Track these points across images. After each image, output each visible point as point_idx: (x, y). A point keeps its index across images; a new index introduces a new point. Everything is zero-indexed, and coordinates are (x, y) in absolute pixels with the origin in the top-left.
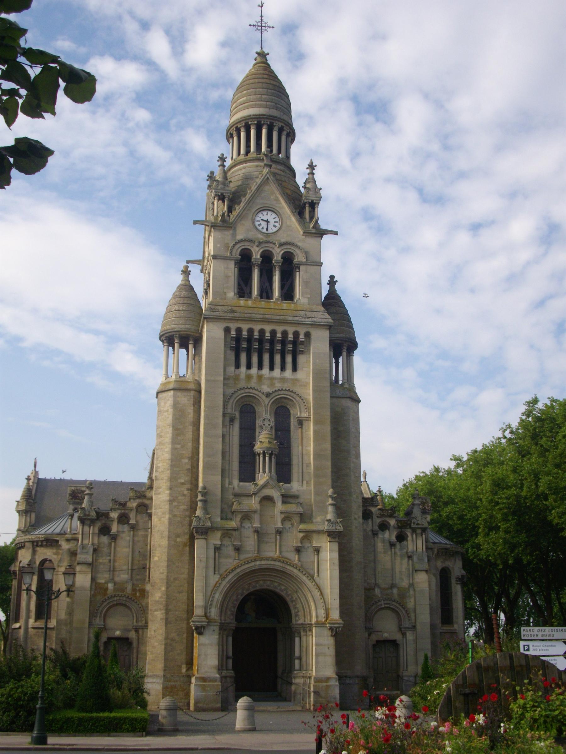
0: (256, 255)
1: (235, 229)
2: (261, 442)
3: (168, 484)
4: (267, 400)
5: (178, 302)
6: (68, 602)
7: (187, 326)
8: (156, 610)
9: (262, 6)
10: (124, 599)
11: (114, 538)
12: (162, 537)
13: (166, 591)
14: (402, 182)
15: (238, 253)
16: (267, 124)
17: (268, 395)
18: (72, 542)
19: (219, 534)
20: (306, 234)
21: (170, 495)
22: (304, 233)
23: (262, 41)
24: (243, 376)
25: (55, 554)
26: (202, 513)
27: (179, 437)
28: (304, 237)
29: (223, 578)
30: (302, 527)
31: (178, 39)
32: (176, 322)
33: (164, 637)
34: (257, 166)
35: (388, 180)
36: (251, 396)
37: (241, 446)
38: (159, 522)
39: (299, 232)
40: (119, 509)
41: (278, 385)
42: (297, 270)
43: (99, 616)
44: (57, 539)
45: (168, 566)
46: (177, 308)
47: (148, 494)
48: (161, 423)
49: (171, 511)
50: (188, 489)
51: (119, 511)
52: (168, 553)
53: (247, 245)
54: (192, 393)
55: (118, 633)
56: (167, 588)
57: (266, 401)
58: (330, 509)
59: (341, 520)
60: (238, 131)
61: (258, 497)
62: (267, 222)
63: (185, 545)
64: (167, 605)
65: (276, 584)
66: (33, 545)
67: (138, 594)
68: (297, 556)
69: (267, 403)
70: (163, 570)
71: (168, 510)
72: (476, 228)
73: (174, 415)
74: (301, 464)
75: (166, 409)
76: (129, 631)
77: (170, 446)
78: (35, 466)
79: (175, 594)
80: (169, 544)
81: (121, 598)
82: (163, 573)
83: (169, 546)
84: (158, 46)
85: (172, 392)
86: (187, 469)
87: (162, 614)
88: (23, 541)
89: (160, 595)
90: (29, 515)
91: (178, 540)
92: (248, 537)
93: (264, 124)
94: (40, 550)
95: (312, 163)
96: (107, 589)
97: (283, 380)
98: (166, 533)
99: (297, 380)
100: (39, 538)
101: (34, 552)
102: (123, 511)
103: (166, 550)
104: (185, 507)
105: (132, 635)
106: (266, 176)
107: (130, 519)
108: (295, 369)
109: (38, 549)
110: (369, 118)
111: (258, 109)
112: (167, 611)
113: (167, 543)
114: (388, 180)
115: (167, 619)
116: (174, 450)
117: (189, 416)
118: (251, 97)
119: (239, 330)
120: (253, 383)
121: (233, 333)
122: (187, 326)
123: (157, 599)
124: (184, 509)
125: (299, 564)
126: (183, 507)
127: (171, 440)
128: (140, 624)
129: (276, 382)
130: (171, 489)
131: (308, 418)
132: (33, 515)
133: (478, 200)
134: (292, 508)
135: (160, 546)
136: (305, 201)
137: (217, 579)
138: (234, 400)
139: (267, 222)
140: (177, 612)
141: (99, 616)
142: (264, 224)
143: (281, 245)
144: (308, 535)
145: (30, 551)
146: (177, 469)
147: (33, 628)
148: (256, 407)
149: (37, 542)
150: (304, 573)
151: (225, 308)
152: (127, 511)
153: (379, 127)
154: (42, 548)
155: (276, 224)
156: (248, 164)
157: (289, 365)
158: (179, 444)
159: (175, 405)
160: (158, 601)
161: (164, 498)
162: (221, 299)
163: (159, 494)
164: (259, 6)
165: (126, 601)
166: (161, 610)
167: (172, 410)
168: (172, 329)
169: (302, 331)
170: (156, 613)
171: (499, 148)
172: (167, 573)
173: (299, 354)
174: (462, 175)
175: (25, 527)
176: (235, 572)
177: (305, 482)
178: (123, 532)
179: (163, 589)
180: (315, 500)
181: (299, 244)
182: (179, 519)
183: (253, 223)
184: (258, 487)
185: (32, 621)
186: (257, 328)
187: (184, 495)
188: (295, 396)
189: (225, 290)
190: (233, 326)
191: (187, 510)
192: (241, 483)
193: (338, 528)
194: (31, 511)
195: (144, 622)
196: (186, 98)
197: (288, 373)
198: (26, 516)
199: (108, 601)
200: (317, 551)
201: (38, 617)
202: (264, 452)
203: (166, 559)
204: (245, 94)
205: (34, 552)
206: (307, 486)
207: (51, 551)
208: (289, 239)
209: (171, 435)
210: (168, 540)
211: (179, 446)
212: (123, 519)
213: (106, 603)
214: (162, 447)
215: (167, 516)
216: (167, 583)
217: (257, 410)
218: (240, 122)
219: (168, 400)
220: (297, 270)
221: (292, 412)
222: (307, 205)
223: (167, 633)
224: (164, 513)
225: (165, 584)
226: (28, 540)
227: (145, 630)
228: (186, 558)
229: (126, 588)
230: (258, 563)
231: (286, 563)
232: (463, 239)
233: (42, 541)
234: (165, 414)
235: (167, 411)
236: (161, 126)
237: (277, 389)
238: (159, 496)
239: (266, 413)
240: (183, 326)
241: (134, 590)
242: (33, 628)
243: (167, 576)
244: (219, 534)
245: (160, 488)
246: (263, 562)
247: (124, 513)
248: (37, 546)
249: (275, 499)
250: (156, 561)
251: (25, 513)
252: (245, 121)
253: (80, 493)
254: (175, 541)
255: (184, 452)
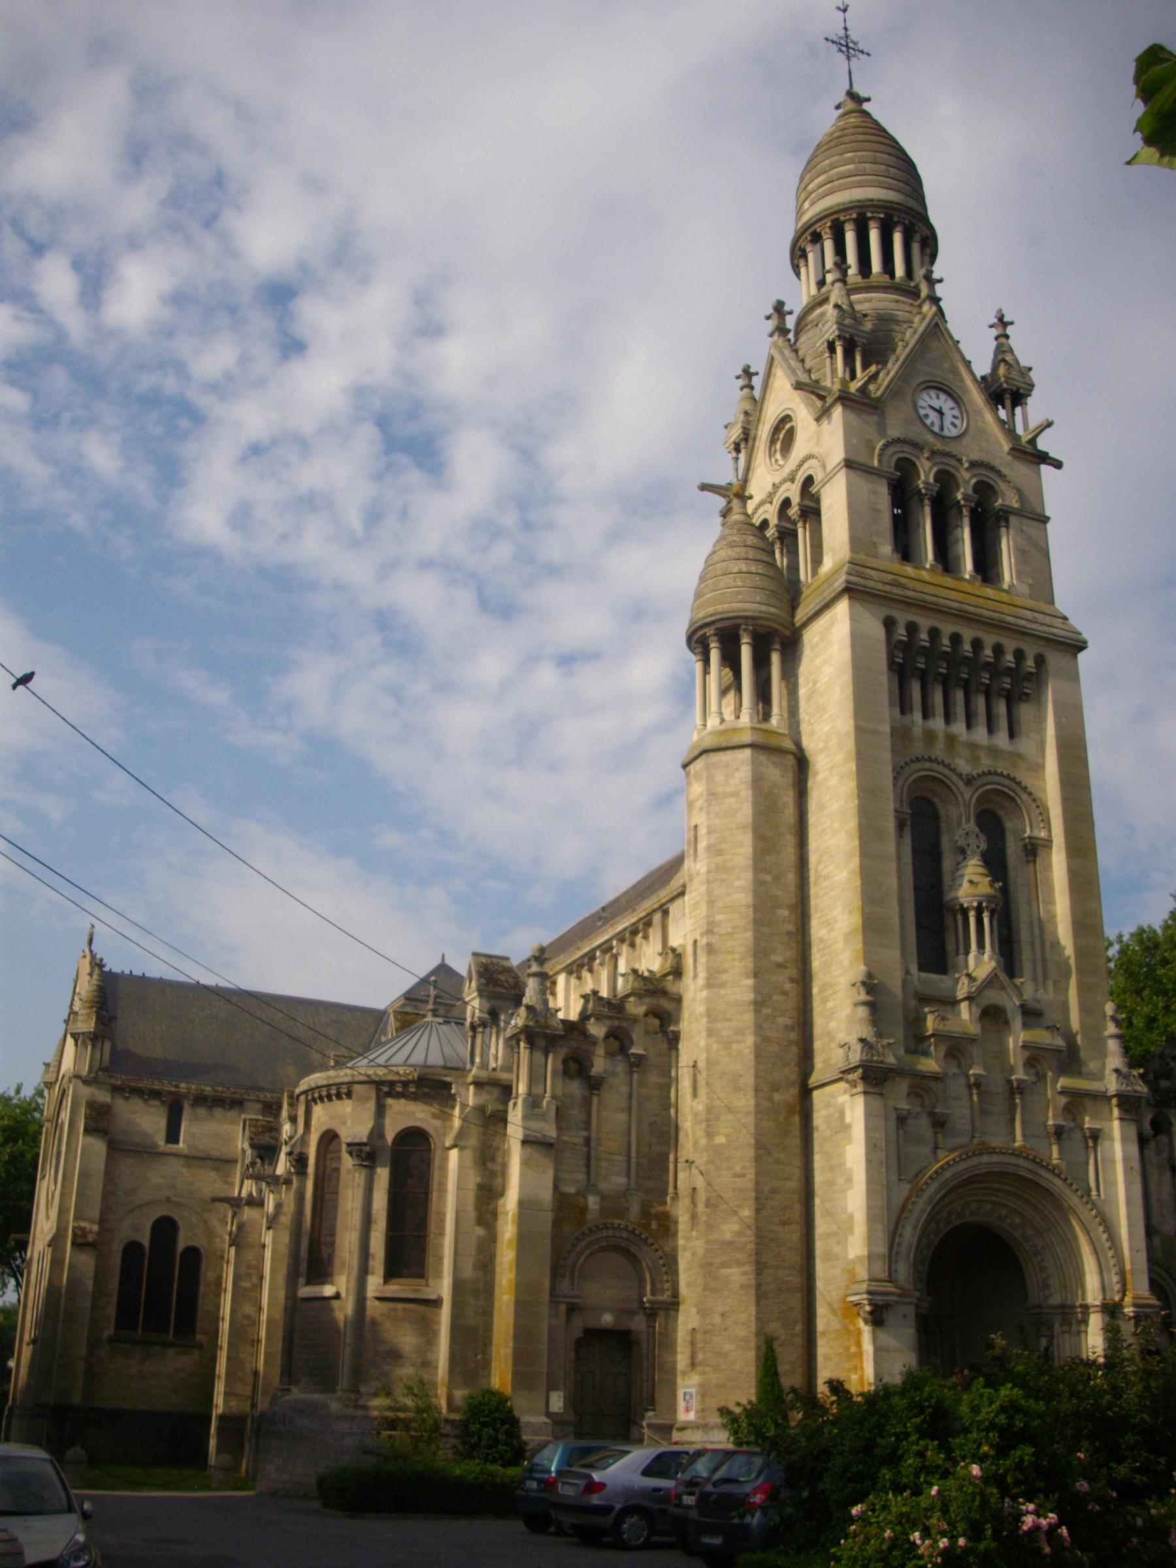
0: (926, 474)
1: (882, 415)
2: (971, 882)
3: (749, 963)
4: (967, 792)
5: (744, 556)
6: (479, 1237)
7: (772, 610)
8: (724, 1265)
9: (845, 11)
10: (625, 1234)
11: (594, 1085)
12: (738, 1089)
13: (757, 1219)
14: (448, 569)
15: (892, 464)
16: (904, 224)
17: (969, 781)
18: (488, 1088)
19: (903, 1086)
20: (1018, 455)
21: (756, 989)
22: (1013, 449)
23: (850, 73)
24: (917, 731)
25: (434, 1116)
26: (872, 1033)
27: (768, 858)
28: (1009, 458)
29: (918, 1191)
30: (1063, 1082)
31: (94, 280)
32: (747, 599)
33: (753, 1330)
34: (897, 301)
35: (426, 564)
36: (935, 778)
37: (917, 889)
38: (723, 1053)
39: (1001, 446)
40: (610, 1018)
41: (986, 763)
42: (1003, 523)
43: (568, 1275)
44: (448, 1079)
45: (757, 1159)
46: (744, 568)
47: (672, 988)
48: (717, 822)
49: (759, 1028)
50: (792, 980)
51: (608, 1022)
52: (757, 1127)
53: (908, 452)
54: (790, 761)
55: (607, 1319)
56: (758, 1211)
57: (968, 795)
58: (1113, 1046)
59: (1141, 1071)
60: (817, 238)
61: (977, 1006)
62: (940, 412)
63: (791, 1112)
64: (758, 1252)
65: (1004, 1212)
66: (378, 1091)
67: (654, 1225)
68: (1055, 1149)
69: (967, 797)
70: (743, 1167)
71: (752, 1024)
72: (568, 661)
73: (756, 804)
74: (1038, 941)
75: (731, 789)
76: (631, 1313)
77: (749, 876)
78: (90, 941)
79: (775, 1228)
80: (757, 1105)
81: (618, 1234)
82: (743, 1176)
83: (758, 1111)
84: (57, 283)
85: (748, 752)
86: (789, 933)
87: (745, 1273)
88: (346, 1079)
89: (735, 1227)
90: (99, 1045)
91: (777, 1097)
92: (956, 1098)
93: (897, 223)
94: (318, 1110)
95: (1003, 316)
96: (584, 1210)
97: (994, 751)
98: (749, 1079)
99: (1020, 756)
100: (398, 1073)
101: (380, 1111)
102: (616, 1023)
103: (751, 1120)
104: (789, 1022)
105: (638, 1323)
106: (932, 319)
107: (632, 1043)
108: (1012, 734)
109: (390, 1101)
110: (403, 459)
111: (884, 191)
112: (760, 1267)
113: (752, 1102)
114: (426, 564)
115: (758, 1286)
116: (759, 888)
117: (787, 811)
118: (867, 165)
119: (912, 628)
120: (939, 751)
121: (901, 633)
122: (772, 610)
123: (728, 1236)
124: (786, 1027)
125: (1064, 1166)
126: (782, 1021)
127: (750, 862)
128: (660, 1298)
129: (982, 754)
130: (756, 975)
131: (1048, 843)
132: (107, 1046)
133: (577, 617)
134: (1043, 1037)
135: (730, 1110)
136: (1005, 386)
137: (905, 1194)
138: (903, 785)
139: (940, 412)
140: (780, 1272)
141: (568, 1275)
142: (933, 417)
143: (974, 465)
144: (1077, 1101)
145: (371, 1106)
146: (766, 930)
147: (378, 1299)
148: (939, 806)
149: (392, 1084)
150: (1074, 1187)
151: (888, 578)
152: (624, 1024)
153: (416, 476)
154: (402, 1101)
155: (957, 422)
156: (873, 295)
157: (1003, 723)
158: (769, 873)
159: (757, 782)
160: (730, 1243)
161: (738, 997)
162: (869, 556)
163: (723, 985)
164: (838, 8)
165: (627, 1240)
166: (739, 1263)
167: (750, 792)
168: (739, 611)
169: (1031, 652)
170: (725, 1271)
171: (615, 536)
172: (758, 1174)
173: (1020, 700)
174: (552, 571)
175: (90, 1071)
176: (942, 1179)
177: (1050, 983)
178: (614, 1074)
179: (747, 1212)
180: (1083, 1025)
181: (1005, 471)
182: (776, 1049)
183: (915, 407)
184: (979, 982)
185: (375, 1283)
186: (947, 629)
187: (785, 993)
188: (1018, 790)
189: (874, 539)
190: (902, 617)
191: (792, 1028)
192: (923, 975)
193: (1138, 1088)
194: (103, 1037)
195: (669, 1293)
196: (92, 381)
197: (1001, 739)
198: (94, 1047)
199: (588, 1239)
200: (1096, 1136)
201: (392, 1272)
202: (980, 904)
203: (753, 1141)
204: (851, 158)
205: (380, 1111)
206: (1055, 992)
207: (426, 1108)
208: (984, 458)
209: (750, 850)
210: (756, 1096)
211: (768, 878)
212: (619, 1039)
213: (583, 1244)
214: (724, 876)
215: (750, 1040)
216: (757, 1199)
217: (942, 812)
218: (845, 210)
219: (738, 769)
220: (1003, 523)
221: (1009, 825)
222: (1007, 396)
223: (761, 1320)
224: (739, 1032)
225: (752, 1201)
226: (362, 1078)
227: (672, 1313)
228: (795, 1141)
229: (628, 1209)
230: (985, 1159)
231: (1040, 1164)
232: (547, 677)
233: (405, 1084)
234: (732, 800)
235: (735, 794)
236: (43, 420)
237: (986, 770)
238: (722, 992)
239: (968, 821)
240: (763, 608)
241: (646, 1214)
242: (378, 1299)
243: (757, 1183)
244: (903, 1086)
245: (725, 971)
246: (995, 1158)
247: (618, 1027)
248: (389, 1094)
249: (1010, 1015)
250: (721, 1145)
251: (91, 1040)
252: (858, 210)
253: (500, 973)
254: (770, 1100)
255: (779, 893)
